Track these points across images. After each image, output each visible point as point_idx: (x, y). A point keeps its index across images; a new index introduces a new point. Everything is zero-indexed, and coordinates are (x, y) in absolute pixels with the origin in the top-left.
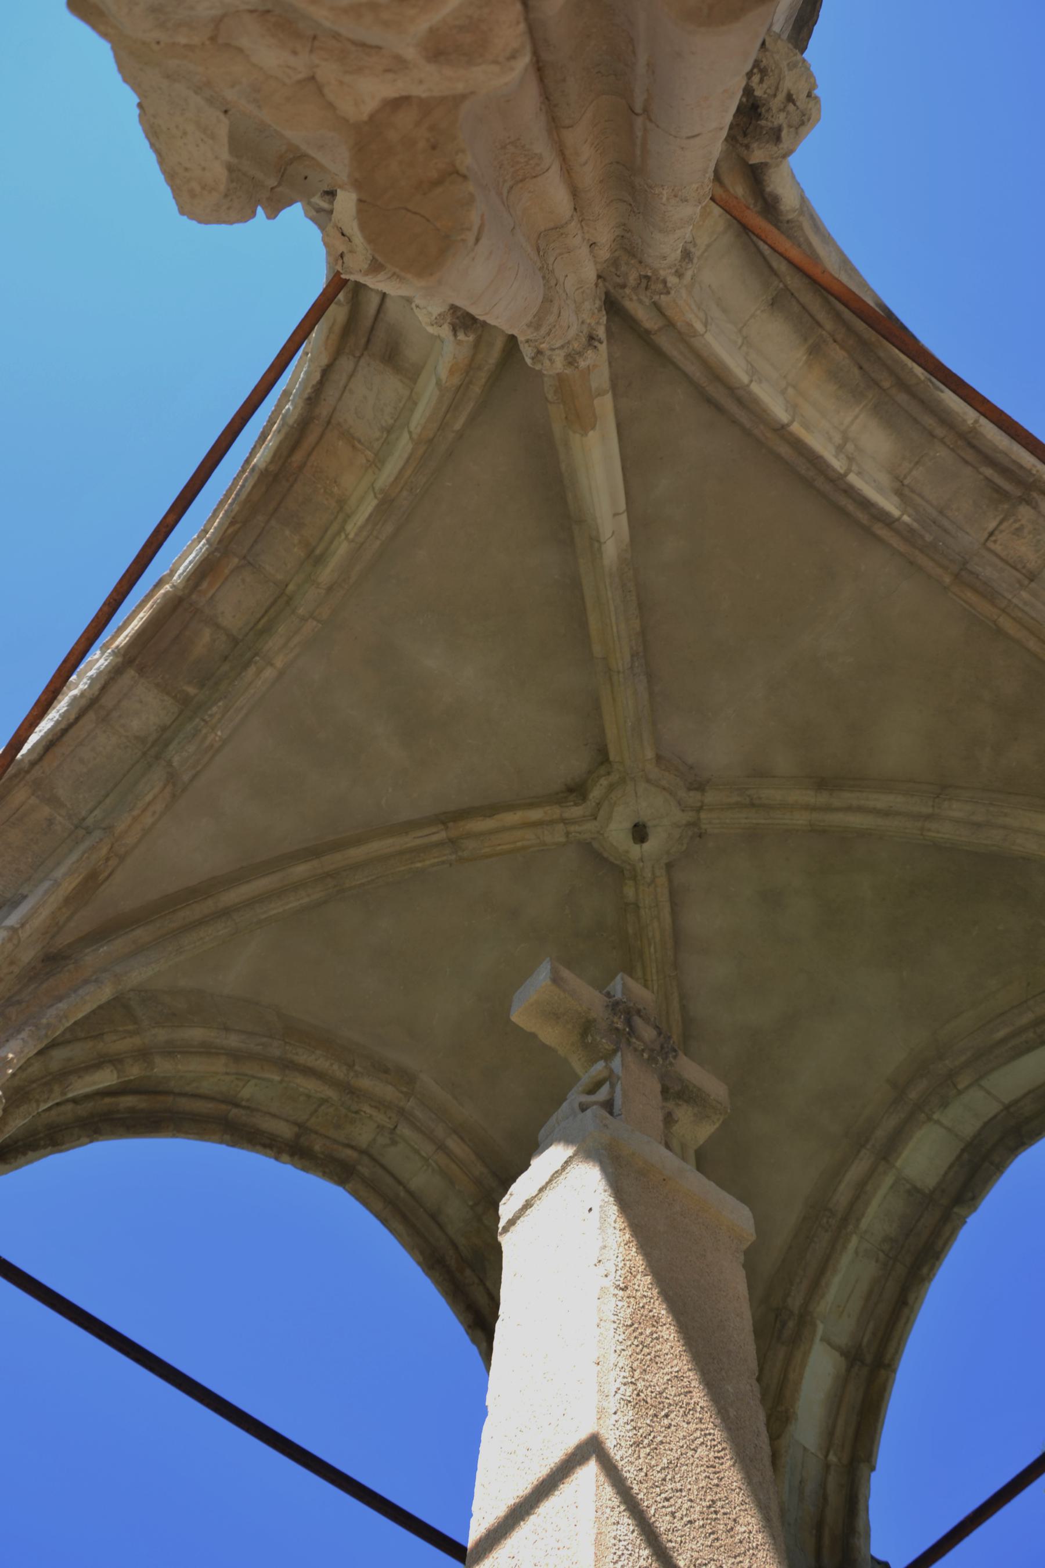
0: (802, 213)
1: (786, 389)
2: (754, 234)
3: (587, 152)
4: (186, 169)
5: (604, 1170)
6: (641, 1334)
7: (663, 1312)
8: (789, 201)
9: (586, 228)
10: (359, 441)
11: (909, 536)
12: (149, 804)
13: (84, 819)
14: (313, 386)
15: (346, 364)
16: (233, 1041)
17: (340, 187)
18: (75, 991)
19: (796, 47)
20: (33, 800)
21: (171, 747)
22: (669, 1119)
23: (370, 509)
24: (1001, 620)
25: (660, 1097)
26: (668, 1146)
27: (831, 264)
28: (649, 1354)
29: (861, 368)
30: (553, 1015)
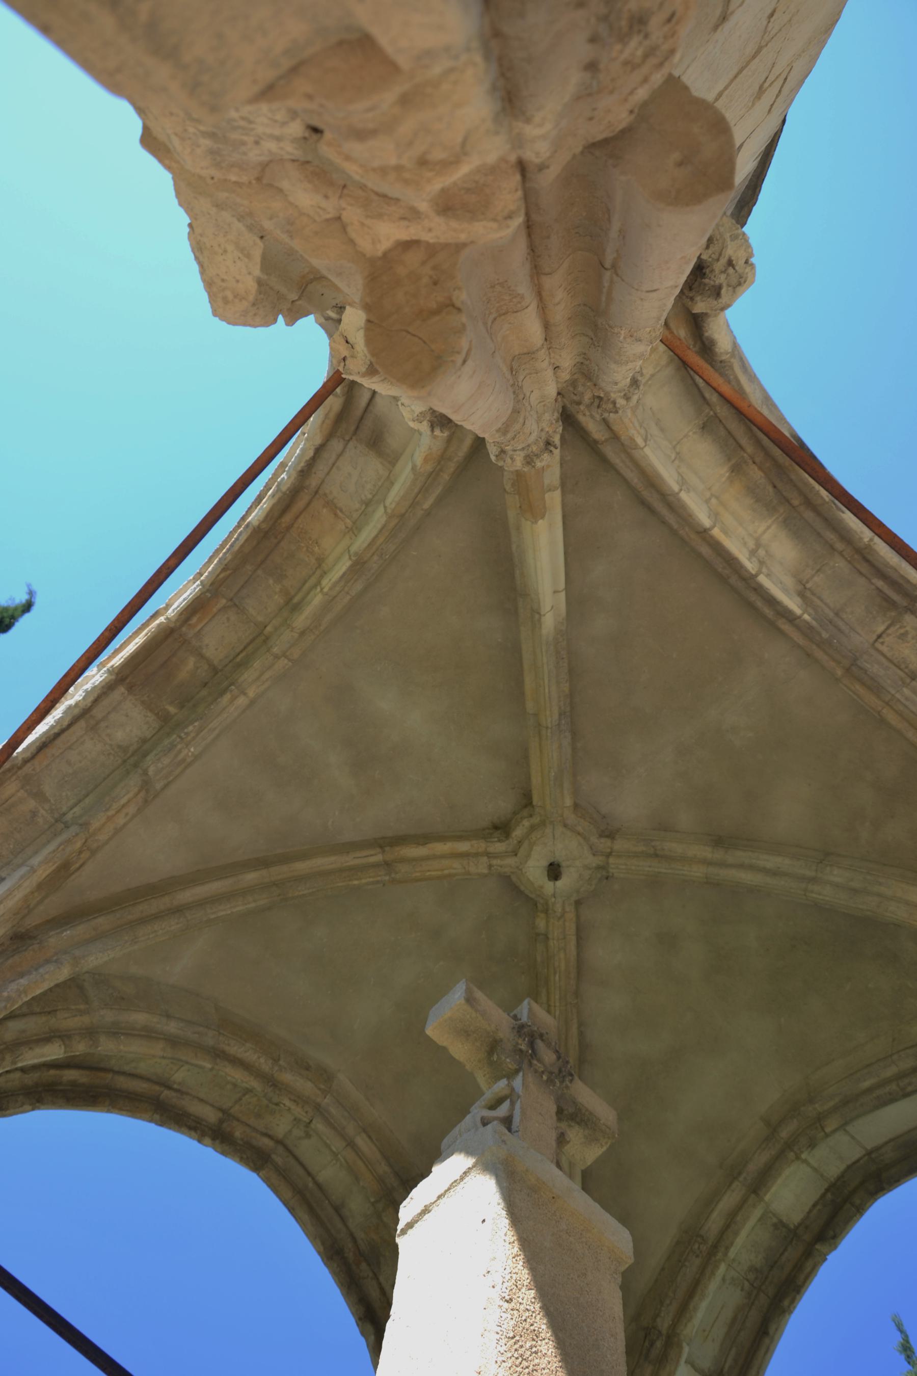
0: (733, 355)
1: (710, 499)
2: (692, 369)
3: (560, 295)
4: (223, 280)
5: (499, 1183)
6: (521, 1347)
7: (544, 1327)
8: (723, 345)
9: (552, 355)
10: (341, 510)
11: (807, 631)
12: (123, 806)
13: (64, 814)
14: (307, 461)
15: (336, 445)
16: (172, 1027)
17: (350, 305)
18: (36, 969)
19: (738, 222)
20: (22, 793)
21: (148, 758)
22: (561, 1139)
23: (344, 569)
24: (884, 711)
25: (555, 1118)
26: (559, 1165)
27: (755, 399)
28: (527, 1367)
29: (775, 487)
30: (464, 1032)
